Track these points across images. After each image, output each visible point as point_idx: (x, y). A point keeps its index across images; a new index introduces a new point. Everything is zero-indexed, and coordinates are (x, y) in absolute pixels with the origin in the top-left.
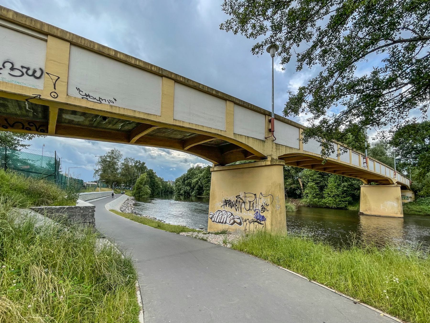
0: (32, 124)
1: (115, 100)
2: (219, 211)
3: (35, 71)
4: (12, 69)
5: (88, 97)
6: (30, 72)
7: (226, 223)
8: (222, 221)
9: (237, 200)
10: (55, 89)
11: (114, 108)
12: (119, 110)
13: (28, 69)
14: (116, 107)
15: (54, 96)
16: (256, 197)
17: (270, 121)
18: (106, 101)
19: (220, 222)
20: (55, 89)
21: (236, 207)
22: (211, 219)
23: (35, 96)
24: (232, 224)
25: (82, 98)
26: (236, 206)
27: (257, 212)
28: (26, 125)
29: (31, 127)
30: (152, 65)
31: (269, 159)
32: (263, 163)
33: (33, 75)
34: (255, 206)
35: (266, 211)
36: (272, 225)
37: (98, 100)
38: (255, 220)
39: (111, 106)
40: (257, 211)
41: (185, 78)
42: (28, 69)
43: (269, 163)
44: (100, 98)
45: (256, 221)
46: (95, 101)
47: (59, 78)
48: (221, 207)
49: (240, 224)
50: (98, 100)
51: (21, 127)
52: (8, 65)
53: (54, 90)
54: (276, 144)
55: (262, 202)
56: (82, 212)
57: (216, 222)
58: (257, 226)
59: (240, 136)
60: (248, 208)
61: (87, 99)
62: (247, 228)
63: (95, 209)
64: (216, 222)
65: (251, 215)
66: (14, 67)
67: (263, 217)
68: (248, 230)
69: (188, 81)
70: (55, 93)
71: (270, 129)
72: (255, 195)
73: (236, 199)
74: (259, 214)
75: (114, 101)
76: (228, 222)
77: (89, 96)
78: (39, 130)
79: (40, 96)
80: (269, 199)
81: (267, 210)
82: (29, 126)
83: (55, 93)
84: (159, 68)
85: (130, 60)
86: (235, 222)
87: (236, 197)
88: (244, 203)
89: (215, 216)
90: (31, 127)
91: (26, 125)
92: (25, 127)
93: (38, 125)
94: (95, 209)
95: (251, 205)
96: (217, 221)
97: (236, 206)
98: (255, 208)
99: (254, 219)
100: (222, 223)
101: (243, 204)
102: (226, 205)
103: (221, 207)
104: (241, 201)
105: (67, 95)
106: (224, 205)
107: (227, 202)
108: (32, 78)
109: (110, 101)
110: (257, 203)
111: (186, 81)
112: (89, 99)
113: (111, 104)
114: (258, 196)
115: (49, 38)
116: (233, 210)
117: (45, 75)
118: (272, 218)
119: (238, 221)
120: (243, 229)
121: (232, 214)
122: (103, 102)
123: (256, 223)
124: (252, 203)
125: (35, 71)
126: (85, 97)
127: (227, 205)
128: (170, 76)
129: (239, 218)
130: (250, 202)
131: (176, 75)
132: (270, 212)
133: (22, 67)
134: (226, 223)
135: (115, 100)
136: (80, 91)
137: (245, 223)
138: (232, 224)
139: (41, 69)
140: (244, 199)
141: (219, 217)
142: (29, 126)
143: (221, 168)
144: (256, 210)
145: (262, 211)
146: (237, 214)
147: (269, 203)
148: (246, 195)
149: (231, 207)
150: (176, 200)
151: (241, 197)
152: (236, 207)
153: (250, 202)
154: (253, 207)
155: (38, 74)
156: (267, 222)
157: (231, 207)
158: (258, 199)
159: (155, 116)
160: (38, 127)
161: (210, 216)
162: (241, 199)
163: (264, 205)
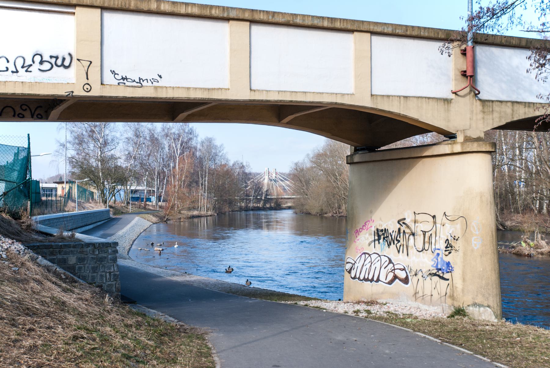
0: (24, 107)
1: (160, 77)
2: (365, 253)
3: (64, 59)
4: (41, 62)
5: (125, 81)
6: (59, 62)
7: (378, 280)
8: (370, 278)
9: (399, 229)
10: (87, 79)
11: (159, 90)
12: (167, 92)
13: (57, 58)
14: (162, 87)
15: (87, 89)
16: (435, 223)
17: (464, 53)
18: (149, 81)
19: (366, 280)
20: (87, 79)
21: (398, 245)
22: (350, 272)
23: (67, 94)
24: (390, 283)
25: (119, 84)
26: (399, 241)
27: (438, 254)
28: (18, 110)
29: (24, 113)
30: (211, 7)
31: (460, 138)
32: (445, 148)
33: (63, 65)
34: (433, 241)
35: (453, 251)
36: (464, 280)
37: (137, 83)
38: (434, 271)
39: (156, 88)
40: (437, 251)
41: (268, 12)
42: (57, 58)
43: (458, 148)
44: (140, 79)
45: (435, 275)
46: (134, 84)
47: (91, 62)
48: (369, 245)
49: (406, 281)
50: (137, 83)
51: (13, 114)
52: (38, 59)
53: (86, 81)
54: (483, 102)
55: (445, 232)
56: (97, 252)
57: (359, 278)
58: (438, 286)
59: (385, 98)
60: (420, 246)
61: (125, 84)
62: (419, 289)
63: (118, 248)
64: (359, 278)
65: (425, 262)
66: (44, 60)
67: (448, 264)
68: (421, 294)
69: (273, 16)
70: (88, 84)
71: (465, 72)
72: (434, 217)
73: (398, 226)
74: (442, 259)
75: (158, 78)
76: (382, 278)
77: (127, 79)
78: (35, 116)
79: (73, 92)
80: (459, 226)
81: (456, 250)
82: (21, 112)
83: (88, 84)
84: (224, 7)
85: (179, 10)
86: (395, 277)
87: (399, 222)
88: (413, 234)
89: (356, 265)
90: (24, 113)
91: (18, 110)
92: (17, 113)
93: (33, 107)
94: (118, 248)
95: (427, 240)
96: (362, 278)
97: (399, 241)
98: (433, 247)
99: (431, 268)
100: (372, 280)
101: (411, 237)
102: (379, 240)
103: (369, 245)
104: (407, 231)
105: (102, 84)
106: (375, 240)
107: (380, 233)
108: (62, 68)
109: (153, 80)
110: (438, 234)
111: (270, 17)
112: (127, 84)
113: (155, 84)
114: (438, 220)
115: (78, 10)
116: (391, 252)
117: (75, 61)
118: (464, 266)
119: (402, 275)
120: (412, 292)
121: (390, 262)
122: (145, 83)
123: (436, 278)
124: (427, 235)
125: (64, 59)
126: (122, 81)
127: (381, 241)
128: (241, 16)
129: (404, 269)
130: (424, 233)
131: (253, 10)
132: (461, 253)
133: (51, 57)
134: (378, 280)
135: (160, 77)
136: (115, 74)
137: (415, 279)
138: (390, 283)
139: (70, 54)
140: (412, 225)
141: (364, 268)
142: (21, 112)
143: (367, 156)
144: (435, 249)
145: (447, 253)
146: (400, 259)
147: (458, 234)
148: (418, 217)
149: (389, 245)
150: (198, 231)
151: (406, 221)
152: (398, 245)
153: (424, 233)
154: (430, 243)
155: (67, 63)
156: (454, 273)
157: (389, 245)
158: (438, 226)
159: (220, 91)
160: (33, 112)
161: (348, 266)
162: (408, 227)
163: (449, 238)
